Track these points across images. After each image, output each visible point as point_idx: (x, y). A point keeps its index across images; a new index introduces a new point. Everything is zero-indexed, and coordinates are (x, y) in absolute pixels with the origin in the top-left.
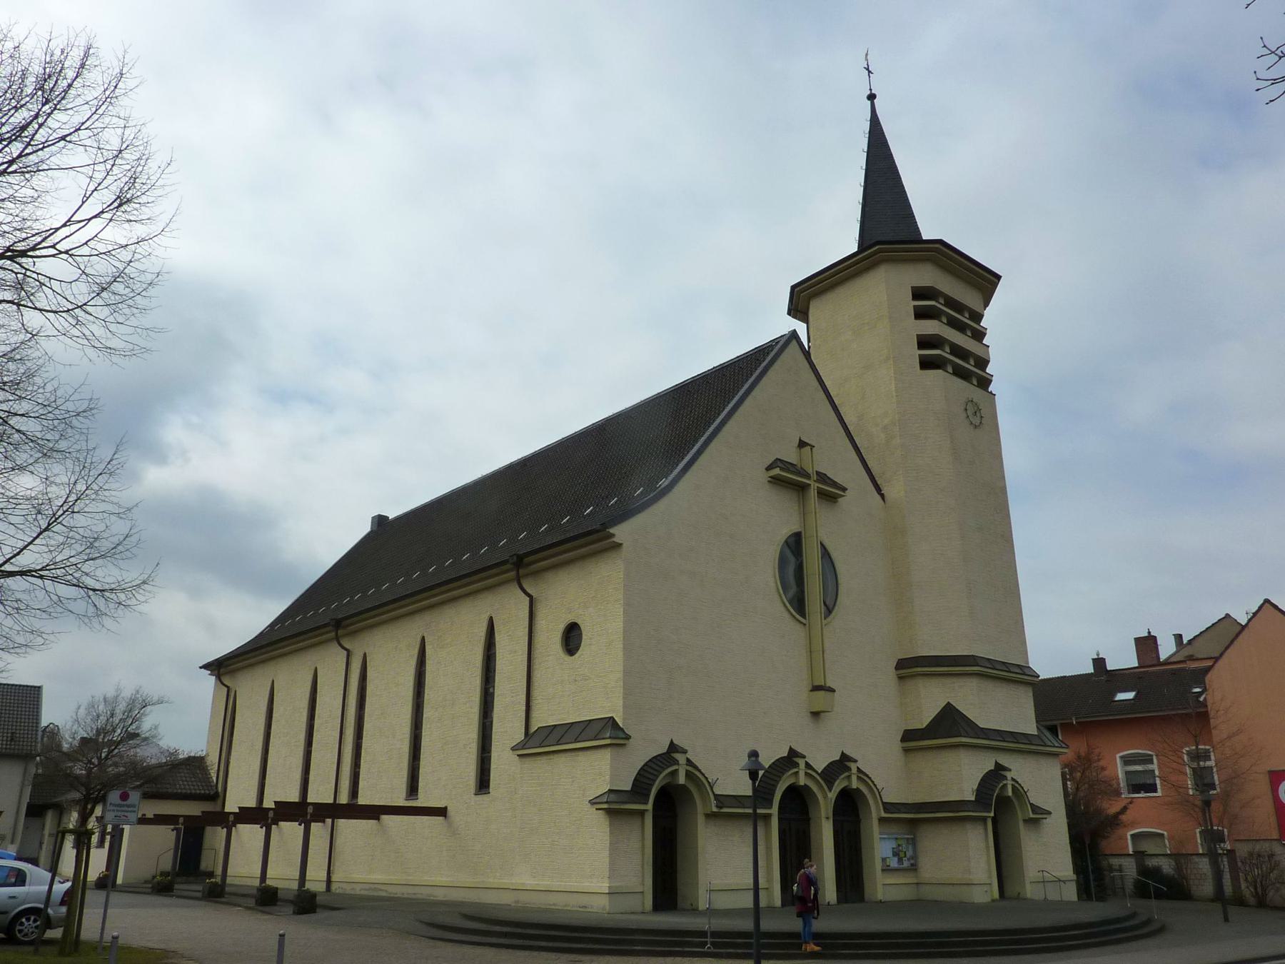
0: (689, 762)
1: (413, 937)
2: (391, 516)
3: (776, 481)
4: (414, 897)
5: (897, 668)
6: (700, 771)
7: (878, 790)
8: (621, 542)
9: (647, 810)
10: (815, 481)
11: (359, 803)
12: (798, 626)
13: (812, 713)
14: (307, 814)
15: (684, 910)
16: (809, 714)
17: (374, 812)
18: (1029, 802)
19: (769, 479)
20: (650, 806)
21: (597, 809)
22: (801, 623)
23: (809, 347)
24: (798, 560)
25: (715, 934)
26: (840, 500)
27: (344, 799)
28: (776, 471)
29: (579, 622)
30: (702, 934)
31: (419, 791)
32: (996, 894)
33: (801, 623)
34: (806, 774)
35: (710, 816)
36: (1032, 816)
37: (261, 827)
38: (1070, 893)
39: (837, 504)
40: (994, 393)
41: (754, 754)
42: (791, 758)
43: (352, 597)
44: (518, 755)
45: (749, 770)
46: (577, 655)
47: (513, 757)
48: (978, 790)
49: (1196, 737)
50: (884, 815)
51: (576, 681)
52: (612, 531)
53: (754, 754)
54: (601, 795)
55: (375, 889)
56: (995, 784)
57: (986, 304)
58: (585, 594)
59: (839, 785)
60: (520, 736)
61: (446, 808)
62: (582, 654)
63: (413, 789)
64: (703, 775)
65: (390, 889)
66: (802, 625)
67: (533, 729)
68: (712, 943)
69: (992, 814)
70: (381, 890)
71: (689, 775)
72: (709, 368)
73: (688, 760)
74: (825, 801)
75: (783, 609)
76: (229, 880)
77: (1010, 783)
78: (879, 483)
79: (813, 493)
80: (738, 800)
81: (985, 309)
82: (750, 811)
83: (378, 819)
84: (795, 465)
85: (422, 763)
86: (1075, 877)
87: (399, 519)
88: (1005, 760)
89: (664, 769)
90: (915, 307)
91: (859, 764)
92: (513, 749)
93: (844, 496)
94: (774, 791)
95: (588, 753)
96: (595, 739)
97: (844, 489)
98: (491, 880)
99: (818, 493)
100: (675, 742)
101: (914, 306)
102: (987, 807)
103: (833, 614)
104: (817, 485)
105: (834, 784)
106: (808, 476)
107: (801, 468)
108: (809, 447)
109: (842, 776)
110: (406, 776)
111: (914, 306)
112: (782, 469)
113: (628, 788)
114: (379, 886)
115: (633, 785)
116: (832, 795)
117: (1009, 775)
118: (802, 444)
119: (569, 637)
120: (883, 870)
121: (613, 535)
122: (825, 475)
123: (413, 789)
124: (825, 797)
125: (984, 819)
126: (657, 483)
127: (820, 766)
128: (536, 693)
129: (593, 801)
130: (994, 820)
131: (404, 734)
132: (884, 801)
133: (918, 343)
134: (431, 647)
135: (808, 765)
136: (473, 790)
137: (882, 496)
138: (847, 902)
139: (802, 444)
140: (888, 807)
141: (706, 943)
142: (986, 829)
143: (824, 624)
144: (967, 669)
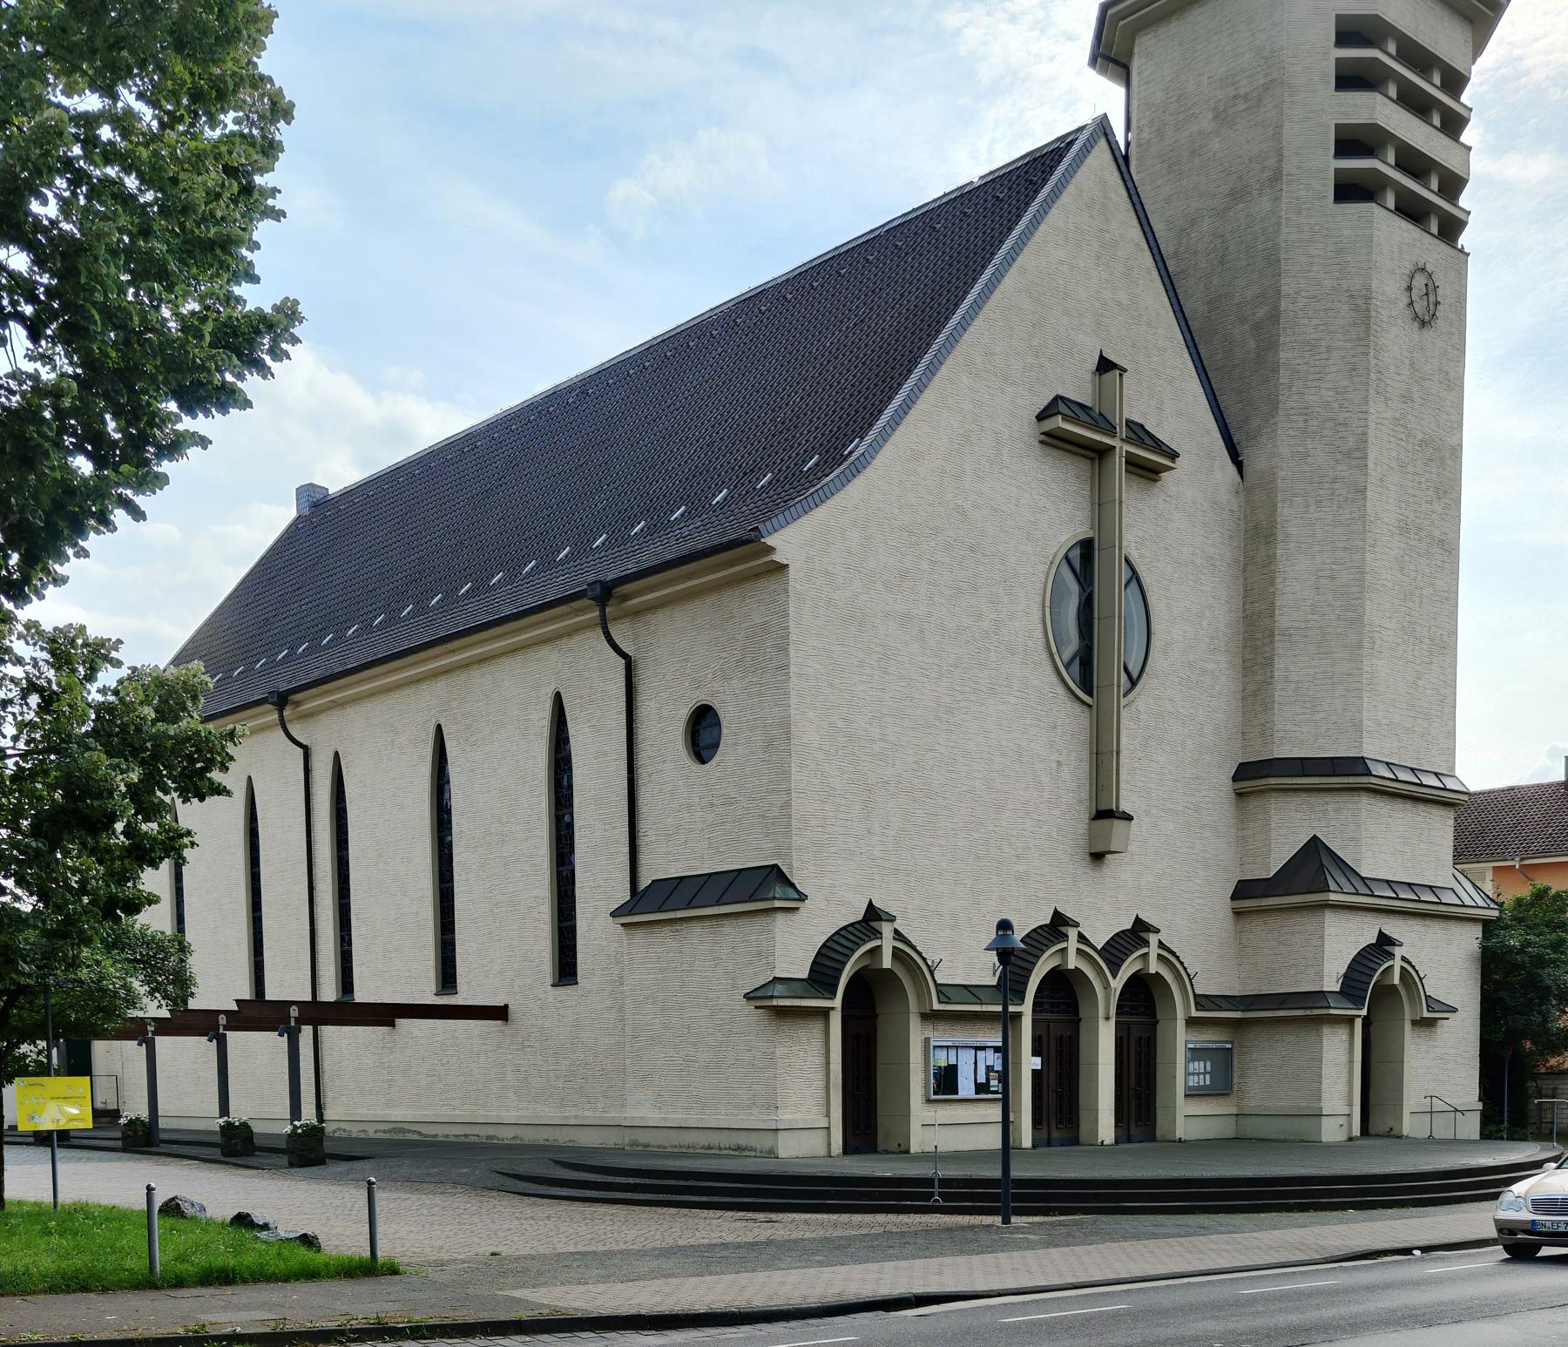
0: (898, 935)
1: (495, 1194)
2: (334, 489)
3: (1054, 440)
4: (463, 1139)
5: (1236, 778)
6: (914, 948)
7: (1189, 975)
8: (785, 562)
9: (833, 1008)
10: (1122, 440)
11: (357, 1001)
12: (1078, 709)
13: (1091, 854)
14: (290, 1017)
15: (887, 1152)
16: (1088, 857)
17: (385, 1015)
18: (935, 981)
19: (1043, 437)
20: (837, 1002)
21: (756, 1007)
22: (1083, 703)
23: (1128, 144)
24: (1085, 591)
25: (945, 1182)
26: (1164, 475)
27: (329, 993)
28: (1058, 422)
29: (716, 705)
30: (928, 1182)
31: (458, 981)
32: (1356, 1131)
33: (1083, 703)
34: (1079, 951)
35: (930, 1017)
36: (1426, 1014)
37: (210, 1041)
38: (1471, 1126)
39: (1158, 484)
40: (1466, 250)
41: (1004, 926)
42: (1058, 924)
43: (293, 649)
44: (622, 925)
45: (997, 949)
46: (714, 762)
47: (614, 926)
48: (1346, 976)
49: (279, 1254)
50: (1194, 1013)
51: (712, 805)
52: (769, 541)
53: (1004, 926)
54: (763, 986)
55: (403, 1131)
56: (1372, 965)
57: (1478, 47)
58: (724, 655)
59: (1128, 969)
60: (625, 896)
61: (506, 1006)
62: (722, 761)
63: (447, 977)
64: (919, 954)
65: (425, 1130)
66: (1085, 708)
67: (644, 883)
68: (940, 1194)
69: (1364, 1012)
70: (409, 1131)
71: (897, 954)
72: (936, 196)
73: (896, 931)
74: (1108, 989)
75: (1054, 679)
76: (162, 1124)
77: (1397, 964)
78: (1235, 440)
79: (1119, 463)
80: (972, 991)
81: (1474, 62)
82: (999, 1008)
83: (392, 1025)
84: (1090, 408)
85: (459, 937)
86: (1480, 1106)
87: (348, 494)
88: (1393, 928)
89: (859, 946)
90: (1339, 61)
91: (1162, 936)
92: (614, 914)
93: (1173, 468)
94: (1028, 977)
95: (741, 921)
96: (751, 899)
97: (1173, 456)
98: (587, 1114)
99: (1126, 462)
100: (877, 904)
101: (1338, 60)
102: (1358, 1001)
103: (1138, 687)
104: (1127, 447)
105: (1120, 966)
106: (1111, 430)
107: (1101, 414)
108: (1118, 372)
109: (1130, 959)
110: (432, 957)
111: (1338, 60)
112: (1066, 418)
113: (804, 974)
114: (406, 1126)
115: (811, 970)
116: (1117, 984)
117: (1398, 951)
118: (1105, 365)
119: (698, 731)
120: (1186, 1096)
121: (771, 550)
122: (1142, 426)
123: (447, 977)
124: (1107, 986)
125: (1350, 1020)
126: (845, 446)
127: (1100, 940)
128: (644, 826)
129: (751, 995)
130: (1367, 1022)
131: (422, 889)
132: (1197, 992)
133: (1337, 142)
134: (454, 743)
135: (1082, 938)
136: (549, 981)
137: (1239, 466)
138: (1129, 1141)
139: (1105, 365)
140: (1203, 1001)
141: (932, 1194)
142: (1352, 1035)
143: (1122, 704)
144: (1352, 780)
